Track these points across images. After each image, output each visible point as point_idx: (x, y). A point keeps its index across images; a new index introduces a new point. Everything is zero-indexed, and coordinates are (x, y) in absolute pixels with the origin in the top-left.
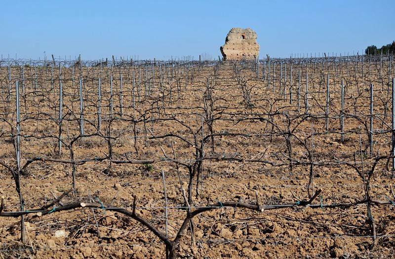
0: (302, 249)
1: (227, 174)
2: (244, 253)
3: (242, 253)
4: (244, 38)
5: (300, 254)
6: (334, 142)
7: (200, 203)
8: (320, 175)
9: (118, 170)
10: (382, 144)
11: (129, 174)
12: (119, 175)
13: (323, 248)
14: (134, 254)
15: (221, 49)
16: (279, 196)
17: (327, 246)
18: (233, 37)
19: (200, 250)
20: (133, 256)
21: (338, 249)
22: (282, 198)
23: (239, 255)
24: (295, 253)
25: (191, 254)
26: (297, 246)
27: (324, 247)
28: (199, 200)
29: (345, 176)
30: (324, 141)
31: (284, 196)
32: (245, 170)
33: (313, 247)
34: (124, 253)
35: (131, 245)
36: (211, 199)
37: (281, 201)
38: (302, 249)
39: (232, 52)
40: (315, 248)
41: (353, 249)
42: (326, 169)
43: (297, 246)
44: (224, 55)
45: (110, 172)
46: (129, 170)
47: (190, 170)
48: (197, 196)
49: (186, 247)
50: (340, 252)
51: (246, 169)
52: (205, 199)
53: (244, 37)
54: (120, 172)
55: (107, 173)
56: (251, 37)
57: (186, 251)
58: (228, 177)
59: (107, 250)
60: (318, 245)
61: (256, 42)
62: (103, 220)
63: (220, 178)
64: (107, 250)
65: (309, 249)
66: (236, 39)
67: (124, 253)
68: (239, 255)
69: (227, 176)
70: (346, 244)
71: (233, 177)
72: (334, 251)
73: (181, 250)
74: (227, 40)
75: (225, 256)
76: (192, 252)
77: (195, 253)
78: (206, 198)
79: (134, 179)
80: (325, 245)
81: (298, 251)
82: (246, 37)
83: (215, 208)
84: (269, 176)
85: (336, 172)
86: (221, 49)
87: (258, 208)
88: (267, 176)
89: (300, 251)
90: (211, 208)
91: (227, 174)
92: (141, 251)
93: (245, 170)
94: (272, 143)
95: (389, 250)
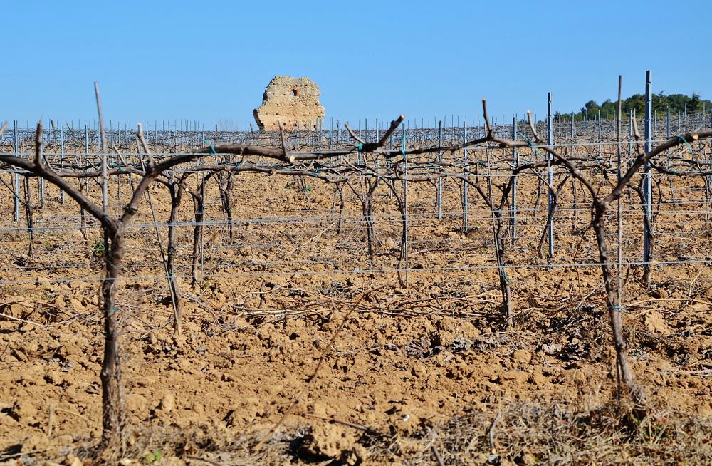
0: (379, 335)
1: (254, 265)
2: (273, 342)
3: (269, 343)
4: (296, 94)
5: (376, 342)
6: (450, 234)
7: (198, 295)
8: (423, 265)
9: (46, 259)
10: (533, 236)
11: (68, 265)
12: (47, 267)
13: (418, 334)
14: (61, 347)
15: (255, 112)
16: (346, 282)
17: (426, 331)
18: (277, 92)
19: (191, 340)
20: (58, 350)
21: (444, 333)
22: (349, 284)
23: (264, 345)
24: (367, 342)
25: (173, 347)
26: (371, 331)
27: (421, 332)
28: (198, 290)
29: (466, 267)
30: (433, 231)
31: (355, 283)
32: (287, 260)
33: (400, 331)
34: (41, 347)
35: (57, 335)
36: (219, 288)
37: (348, 290)
38: (379, 335)
39: (275, 119)
40: (403, 333)
41: (470, 333)
42: (432, 256)
43: (371, 331)
44: (261, 125)
45: (30, 263)
46: (67, 259)
47: (172, 192)
48: (192, 284)
49: (163, 336)
50: (448, 337)
51: (289, 257)
52: (208, 289)
53: (295, 92)
54: (49, 262)
55: (23, 265)
56: (309, 92)
57: (164, 342)
58: (255, 270)
59: (7, 341)
60: (409, 328)
61: (318, 102)
62: (6, 309)
63: (240, 272)
64: (7, 341)
65: (392, 335)
66: (281, 95)
67: (41, 347)
68: (264, 345)
69: (253, 268)
70: (460, 325)
71: (264, 269)
72: (437, 336)
73: (154, 340)
74: (265, 98)
75: (237, 349)
76: (175, 344)
77: (180, 344)
78: (211, 287)
79: (75, 273)
80: (423, 327)
81: (372, 339)
82: (300, 93)
83: (199, 157)
84: (331, 267)
85: (451, 262)
86: (255, 112)
87: (284, 154)
88: (326, 267)
89: (376, 339)
90: (193, 157)
91: (254, 265)
92: (76, 343)
93: (287, 260)
94: (340, 235)
95: (534, 334)
